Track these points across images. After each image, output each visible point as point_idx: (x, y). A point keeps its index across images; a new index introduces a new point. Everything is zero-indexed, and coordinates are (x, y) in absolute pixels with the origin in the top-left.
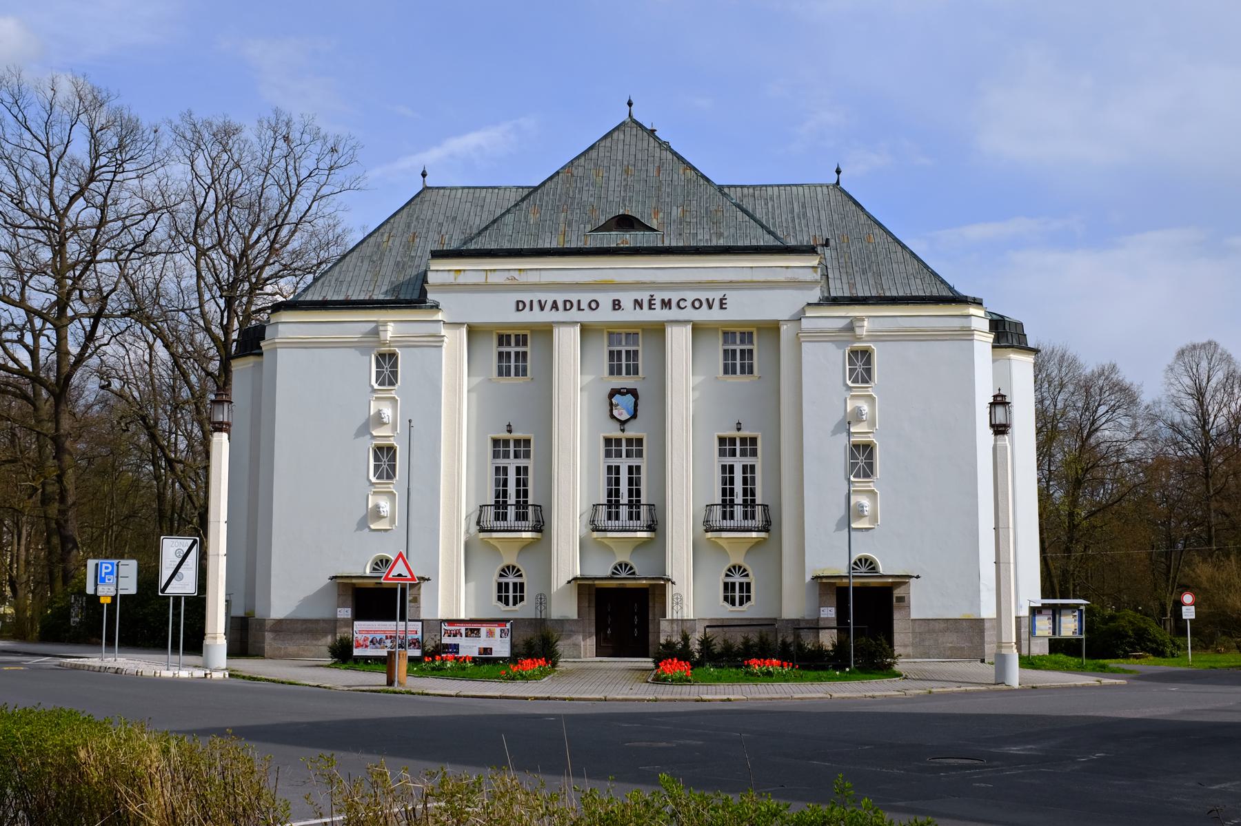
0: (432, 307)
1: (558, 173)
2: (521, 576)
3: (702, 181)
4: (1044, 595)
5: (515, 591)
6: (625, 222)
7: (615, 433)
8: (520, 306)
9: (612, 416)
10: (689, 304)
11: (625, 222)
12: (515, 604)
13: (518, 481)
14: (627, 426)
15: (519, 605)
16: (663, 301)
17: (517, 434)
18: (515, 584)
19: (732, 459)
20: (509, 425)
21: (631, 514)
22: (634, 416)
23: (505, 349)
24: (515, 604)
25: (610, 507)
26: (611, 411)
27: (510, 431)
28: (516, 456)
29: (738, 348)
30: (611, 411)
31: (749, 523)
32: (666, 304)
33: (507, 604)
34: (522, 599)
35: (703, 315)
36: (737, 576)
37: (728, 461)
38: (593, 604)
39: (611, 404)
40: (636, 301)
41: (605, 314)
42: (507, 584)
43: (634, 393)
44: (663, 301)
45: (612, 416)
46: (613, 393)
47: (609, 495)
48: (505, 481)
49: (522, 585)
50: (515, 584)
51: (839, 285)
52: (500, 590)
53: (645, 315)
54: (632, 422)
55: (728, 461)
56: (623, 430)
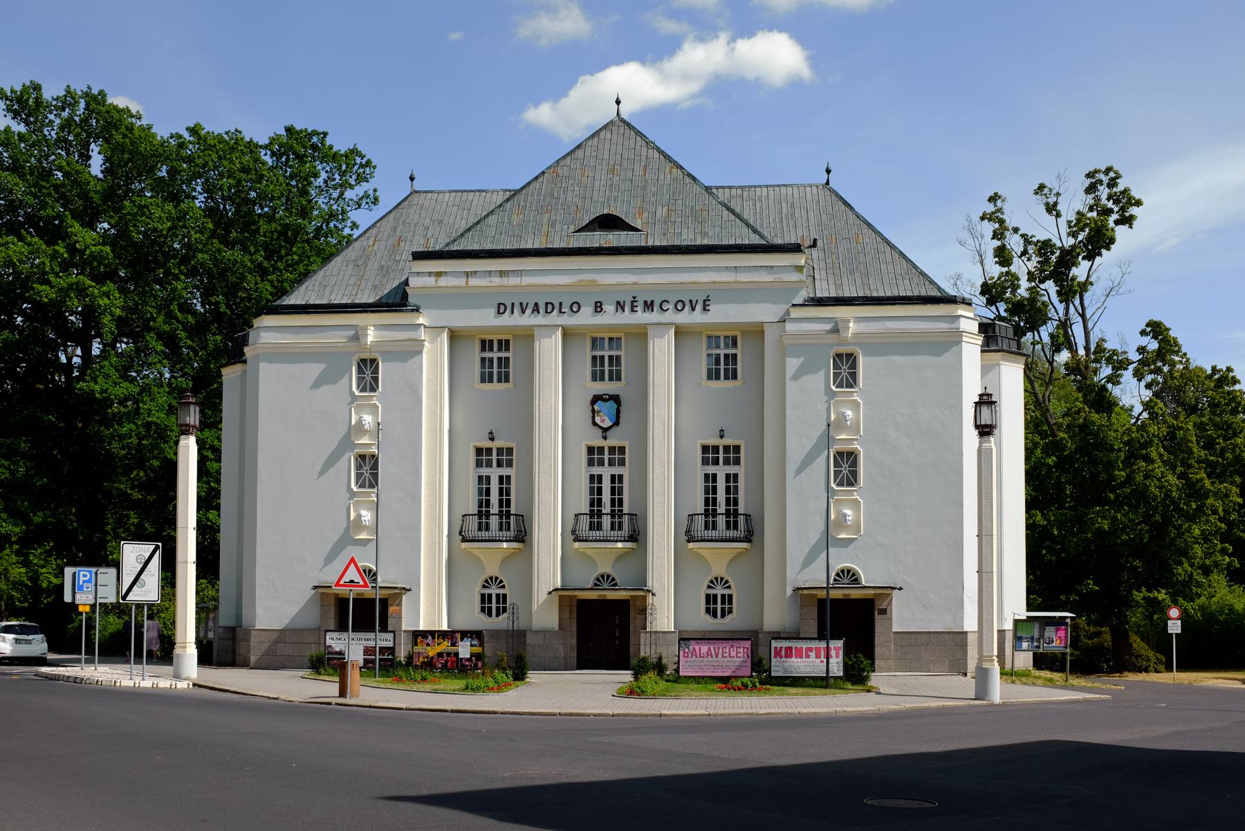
0: (413, 310)
1: (543, 173)
2: (729, 587)
3: (688, 180)
4: (1030, 607)
5: (498, 602)
6: (609, 222)
7: (598, 442)
8: (501, 309)
9: (595, 424)
10: (671, 306)
11: (609, 222)
12: (498, 615)
13: (501, 490)
14: (608, 434)
15: (501, 617)
16: (645, 302)
17: (498, 443)
18: (498, 595)
19: (715, 467)
20: (491, 433)
21: (728, 523)
22: (617, 423)
23: (598, 353)
24: (498, 615)
25: (480, 518)
26: (593, 418)
27: (492, 439)
28: (499, 464)
29: (722, 352)
30: (593, 418)
31: (732, 533)
32: (649, 306)
33: (490, 615)
34: (730, 611)
35: (684, 318)
36: (719, 587)
37: (711, 469)
38: (575, 615)
39: (593, 411)
40: (618, 303)
41: (586, 317)
42: (715, 596)
43: (616, 399)
44: (645, 302)
45: (595, 424)
46: (596, 399)
47: (592, 505)
48: (600, 490)
49: (730, 596)
50: (498, 595)
51: (825, 286)
52: (708, 602)
53: (627, 318)
54: (615, 429)
55: (711, 469)
56: (605, 438)
